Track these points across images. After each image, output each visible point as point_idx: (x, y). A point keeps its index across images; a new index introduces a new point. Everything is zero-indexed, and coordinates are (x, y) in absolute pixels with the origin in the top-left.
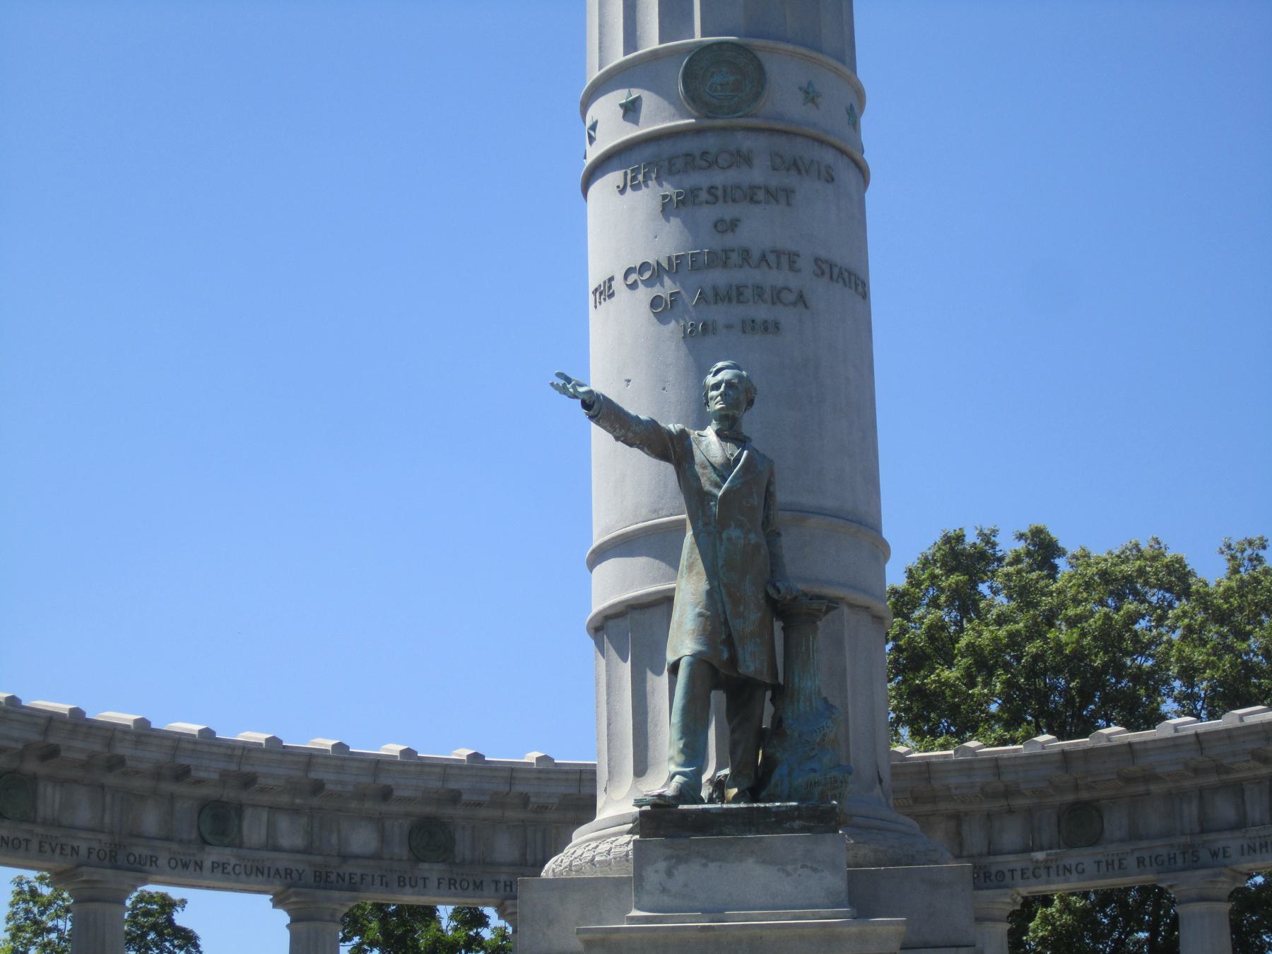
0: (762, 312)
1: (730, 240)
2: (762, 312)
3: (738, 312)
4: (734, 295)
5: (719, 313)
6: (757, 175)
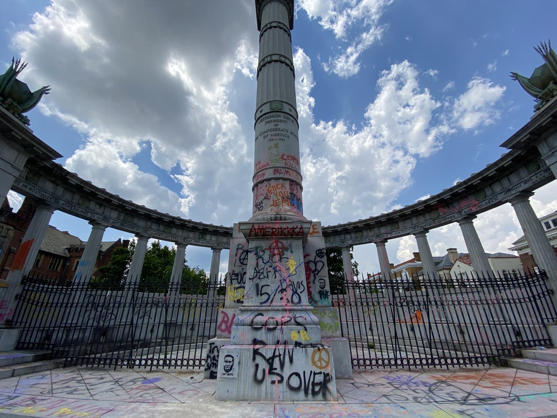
0: (282, 137)
1: (276, 127)
2: (282, 137)
3: (277, 137)
4: (275, 135)
5: (272, 137)
6: (282, 118)
